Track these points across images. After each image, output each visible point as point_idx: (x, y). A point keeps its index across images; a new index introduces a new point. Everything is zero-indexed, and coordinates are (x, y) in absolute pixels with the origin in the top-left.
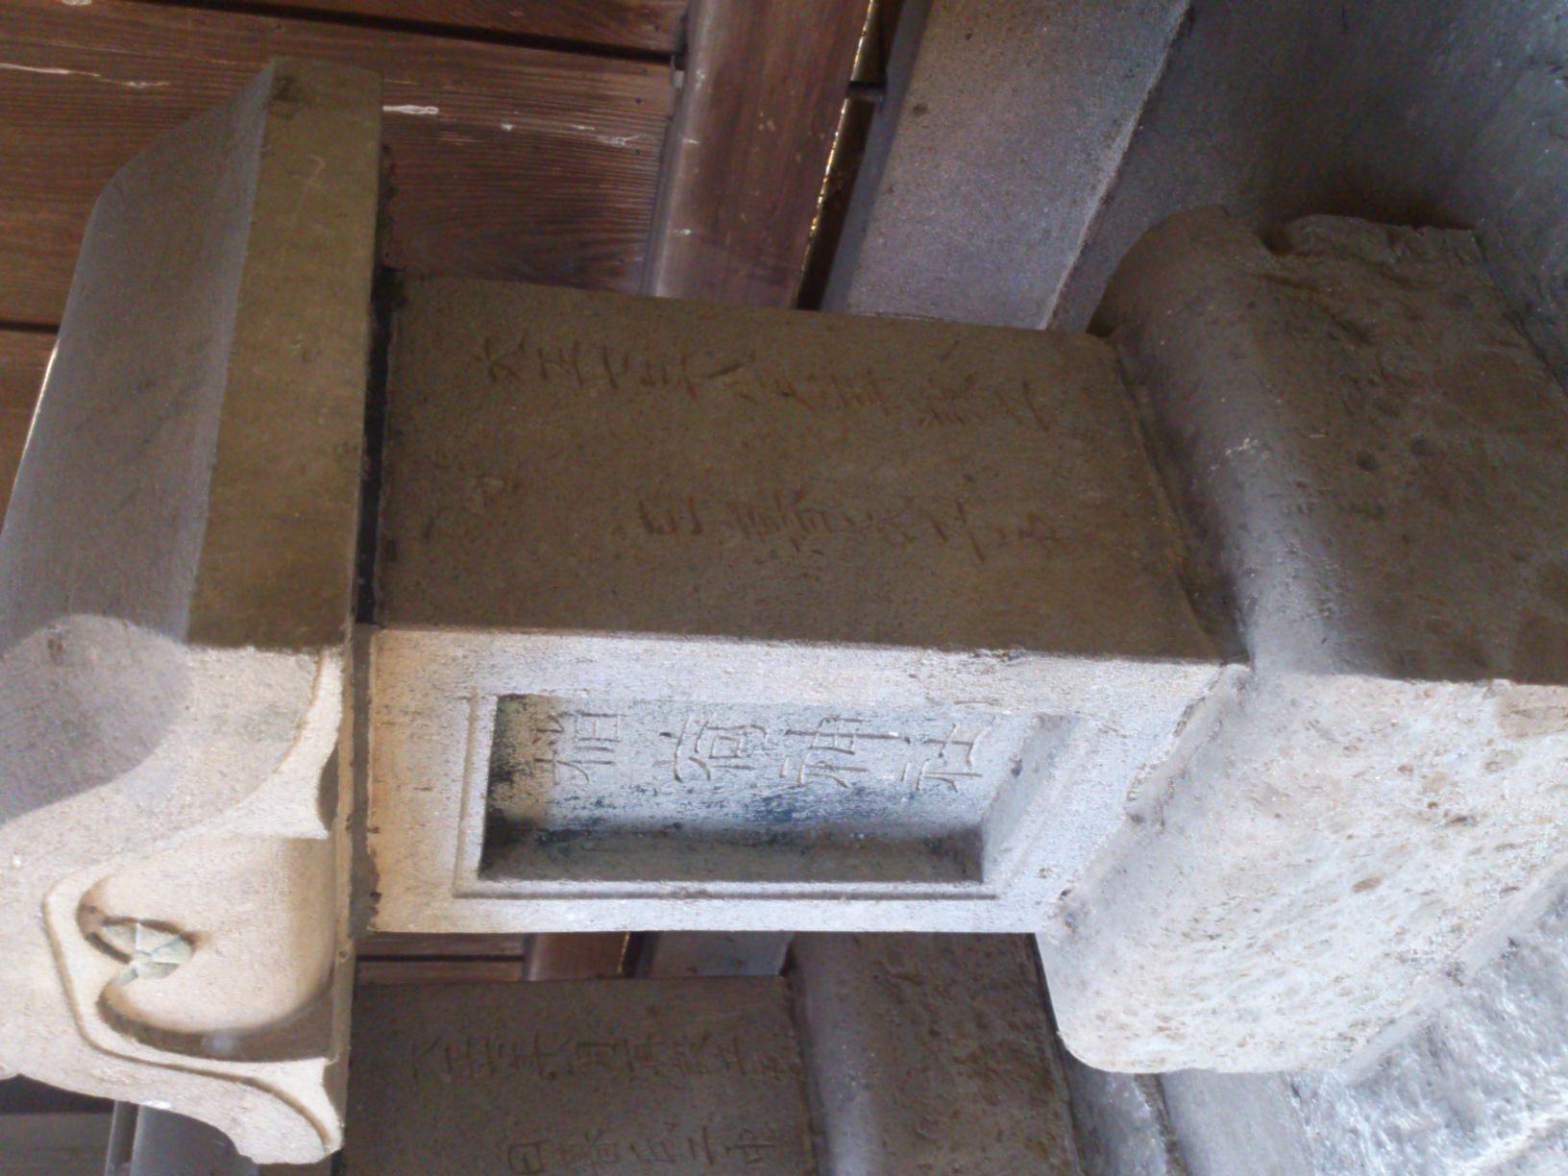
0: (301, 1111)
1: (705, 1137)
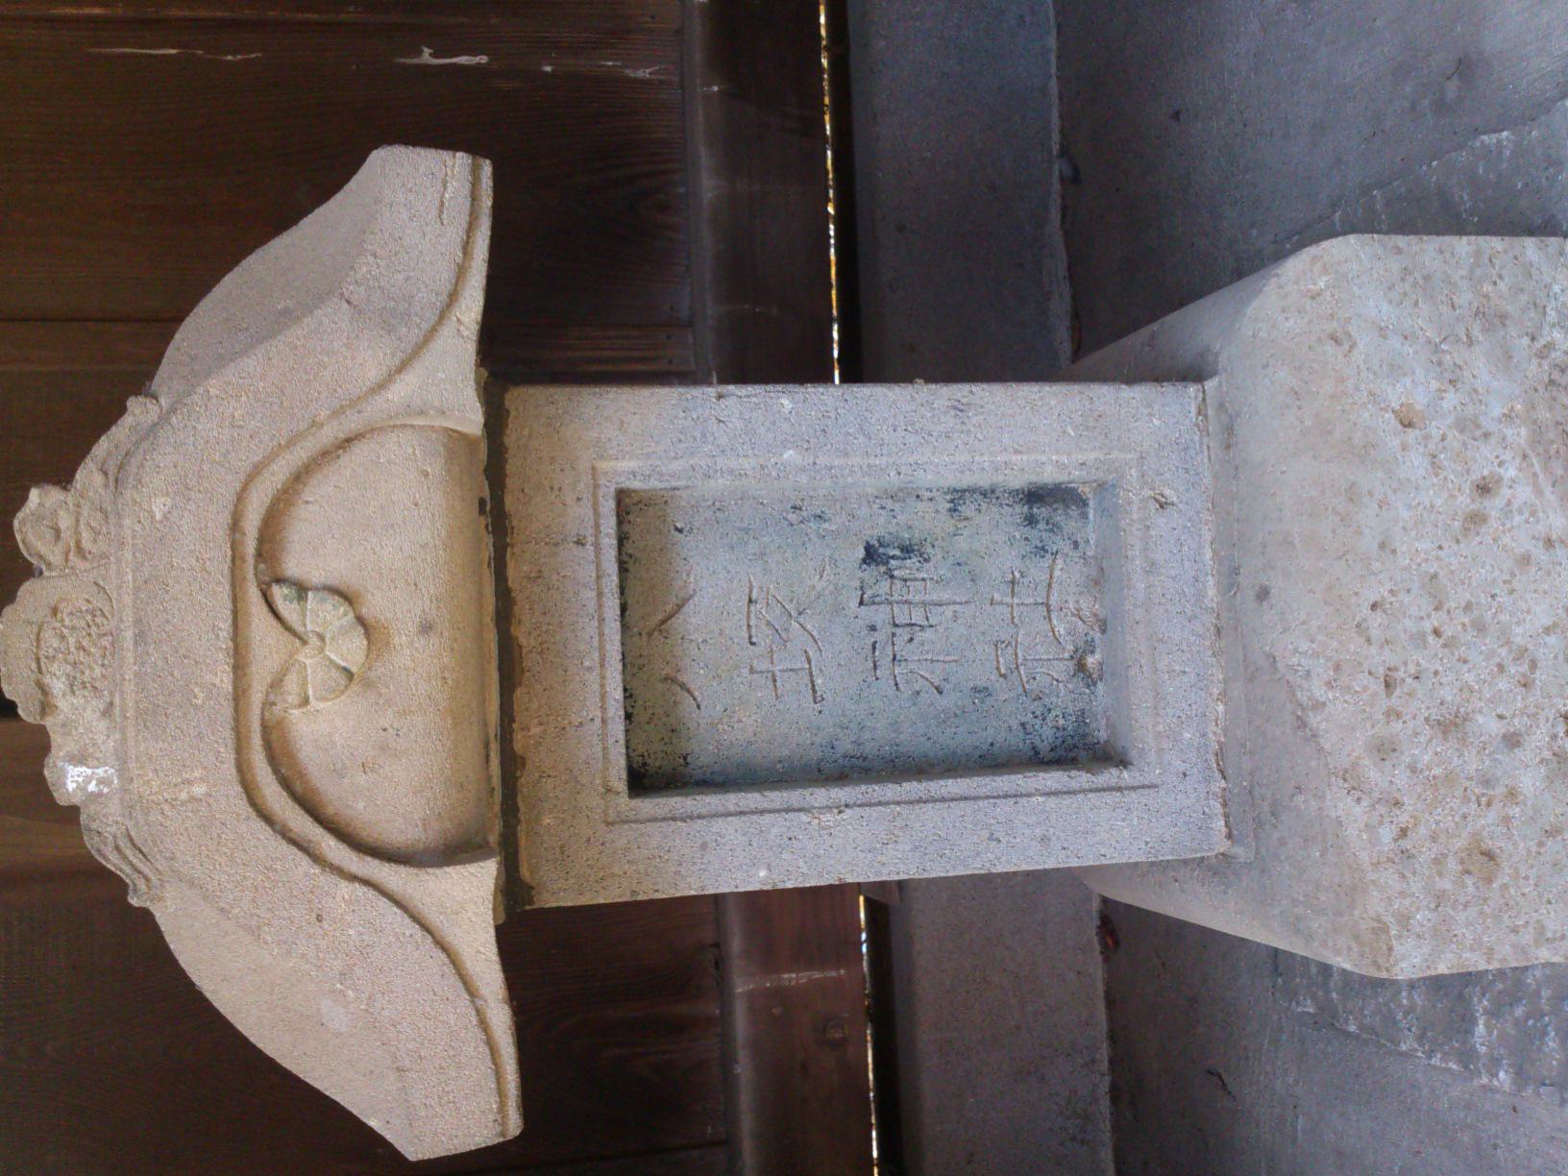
0: (472, 992)
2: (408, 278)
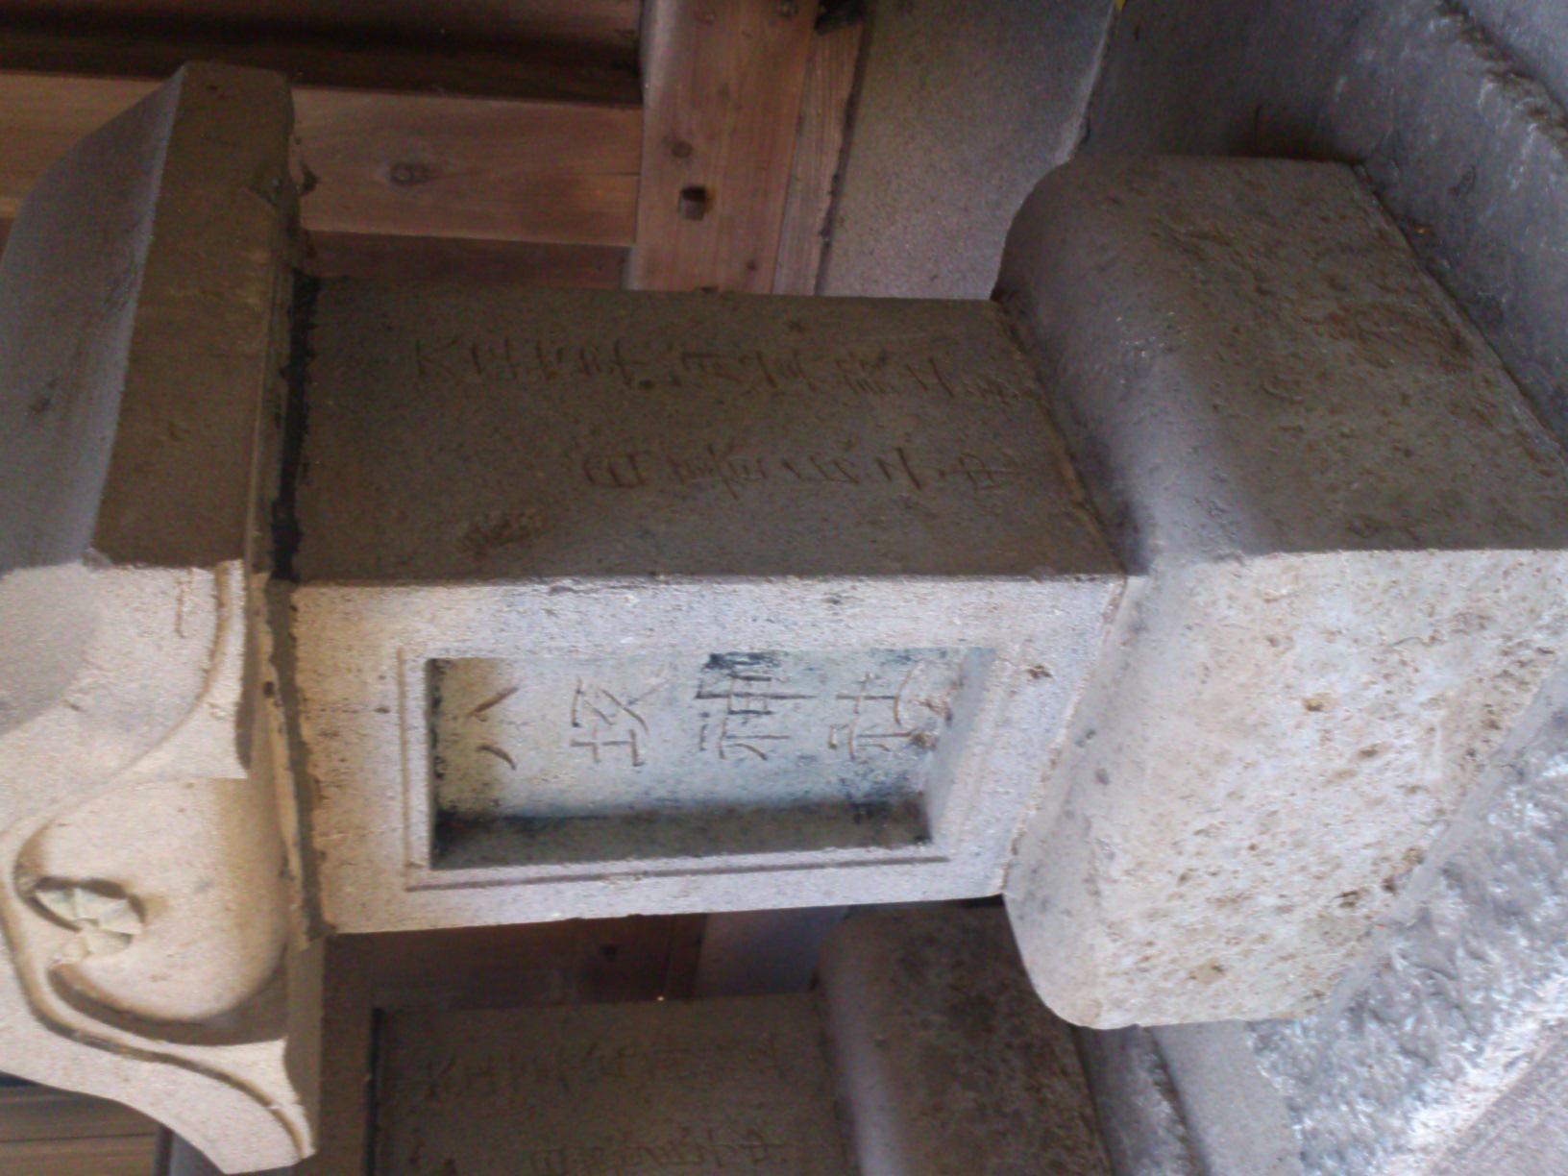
0: (263, 1101)
1: (904, 459)
2: (144, 687)
